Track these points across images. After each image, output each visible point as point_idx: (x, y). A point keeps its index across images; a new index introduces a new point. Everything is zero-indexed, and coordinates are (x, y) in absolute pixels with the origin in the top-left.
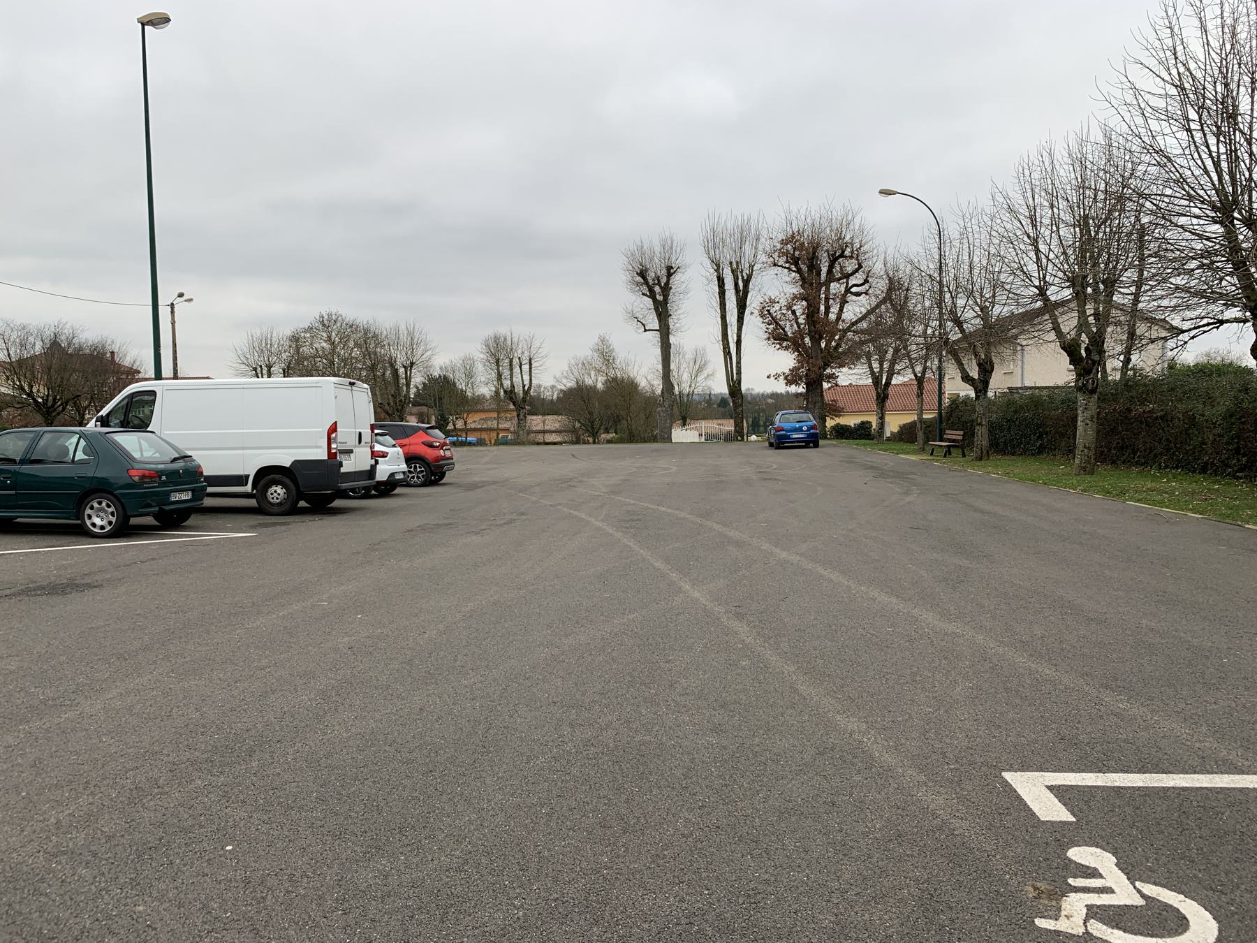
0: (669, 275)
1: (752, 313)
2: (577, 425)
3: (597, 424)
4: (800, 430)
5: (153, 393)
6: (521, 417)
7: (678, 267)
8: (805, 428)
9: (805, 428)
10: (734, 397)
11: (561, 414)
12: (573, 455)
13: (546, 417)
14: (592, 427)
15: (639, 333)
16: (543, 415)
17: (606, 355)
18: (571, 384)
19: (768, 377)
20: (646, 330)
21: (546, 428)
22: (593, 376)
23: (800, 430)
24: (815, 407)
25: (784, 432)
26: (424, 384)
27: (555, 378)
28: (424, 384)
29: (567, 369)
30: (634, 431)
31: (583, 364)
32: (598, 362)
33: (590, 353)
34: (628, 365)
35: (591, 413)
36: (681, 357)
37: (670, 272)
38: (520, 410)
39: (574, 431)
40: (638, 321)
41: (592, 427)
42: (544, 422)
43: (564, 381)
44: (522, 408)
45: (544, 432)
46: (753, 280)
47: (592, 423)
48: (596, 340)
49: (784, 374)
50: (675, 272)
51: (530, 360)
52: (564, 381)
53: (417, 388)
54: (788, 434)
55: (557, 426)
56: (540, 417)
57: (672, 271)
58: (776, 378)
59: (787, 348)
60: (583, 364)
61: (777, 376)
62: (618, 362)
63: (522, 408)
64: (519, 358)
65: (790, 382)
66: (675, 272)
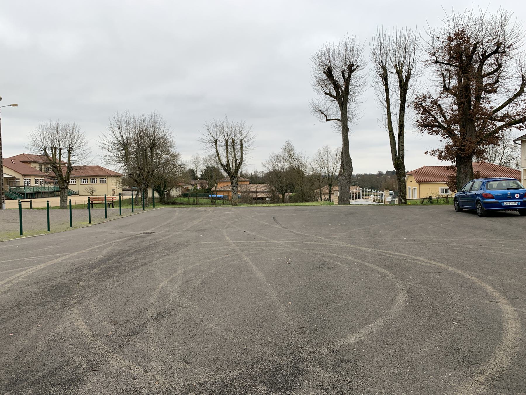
0: (351, 71)
1: (409, 106)
2: (274, 189)
3: (284, 189)
4: (512, 197)
5: (360, 198)
6: (234, 184)
7: (358, 66)
8: (517, 196)
9: (517, 196)
10: (399, 169)
11: (266, 183)
12: (274, 218)
13: (258, 185)
14: (282, 190)
15: (323, 122)
16: (256, 184)
17: (290, 153)
18: (271, 168)
19: (426, 153)
20: (327, 120)
21: (258, 190)
22: (282, 163)
23: (512, 197)
24: (466, 176)
25: (494, 200)
26: (205, 170)
27: (262, 164)
28: (205, 170)
29: (269, 159)
30: (305, 192)
31: (277, 157)
32: (285, 155)
33: (281, 151)
34: (301, 157)
35: (281, 183)
36: (329, 153)
37: (351, 68)
38: (233, 179)
39: (272, 192)
40: (322, 113)
41: (282, 190)
42: (256, 187)
43: (267, 165)
44: (234, 177)
45: (256, 192)
46: (411, 82)
47: (282, 188)
48: (284, 144)
49: (439, 151)
50: (355, 69)
51: (241, 141)
52: (267, 165)
53: (202, 171)
54: (499, 201)
55: (263, 189)
56: (255, 185)
57: (353, 68)
58: (433, 154)
59: (437, 132)
60: (277, 157)
61: (433, 153)
62: (296, 155)
63: (234, 177)
64: (232, 139)
65: (440, 157)
66: (355, 69)
